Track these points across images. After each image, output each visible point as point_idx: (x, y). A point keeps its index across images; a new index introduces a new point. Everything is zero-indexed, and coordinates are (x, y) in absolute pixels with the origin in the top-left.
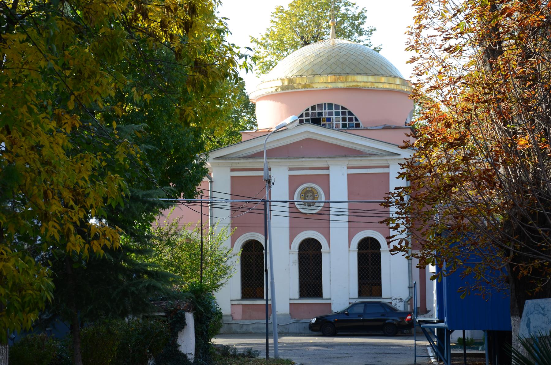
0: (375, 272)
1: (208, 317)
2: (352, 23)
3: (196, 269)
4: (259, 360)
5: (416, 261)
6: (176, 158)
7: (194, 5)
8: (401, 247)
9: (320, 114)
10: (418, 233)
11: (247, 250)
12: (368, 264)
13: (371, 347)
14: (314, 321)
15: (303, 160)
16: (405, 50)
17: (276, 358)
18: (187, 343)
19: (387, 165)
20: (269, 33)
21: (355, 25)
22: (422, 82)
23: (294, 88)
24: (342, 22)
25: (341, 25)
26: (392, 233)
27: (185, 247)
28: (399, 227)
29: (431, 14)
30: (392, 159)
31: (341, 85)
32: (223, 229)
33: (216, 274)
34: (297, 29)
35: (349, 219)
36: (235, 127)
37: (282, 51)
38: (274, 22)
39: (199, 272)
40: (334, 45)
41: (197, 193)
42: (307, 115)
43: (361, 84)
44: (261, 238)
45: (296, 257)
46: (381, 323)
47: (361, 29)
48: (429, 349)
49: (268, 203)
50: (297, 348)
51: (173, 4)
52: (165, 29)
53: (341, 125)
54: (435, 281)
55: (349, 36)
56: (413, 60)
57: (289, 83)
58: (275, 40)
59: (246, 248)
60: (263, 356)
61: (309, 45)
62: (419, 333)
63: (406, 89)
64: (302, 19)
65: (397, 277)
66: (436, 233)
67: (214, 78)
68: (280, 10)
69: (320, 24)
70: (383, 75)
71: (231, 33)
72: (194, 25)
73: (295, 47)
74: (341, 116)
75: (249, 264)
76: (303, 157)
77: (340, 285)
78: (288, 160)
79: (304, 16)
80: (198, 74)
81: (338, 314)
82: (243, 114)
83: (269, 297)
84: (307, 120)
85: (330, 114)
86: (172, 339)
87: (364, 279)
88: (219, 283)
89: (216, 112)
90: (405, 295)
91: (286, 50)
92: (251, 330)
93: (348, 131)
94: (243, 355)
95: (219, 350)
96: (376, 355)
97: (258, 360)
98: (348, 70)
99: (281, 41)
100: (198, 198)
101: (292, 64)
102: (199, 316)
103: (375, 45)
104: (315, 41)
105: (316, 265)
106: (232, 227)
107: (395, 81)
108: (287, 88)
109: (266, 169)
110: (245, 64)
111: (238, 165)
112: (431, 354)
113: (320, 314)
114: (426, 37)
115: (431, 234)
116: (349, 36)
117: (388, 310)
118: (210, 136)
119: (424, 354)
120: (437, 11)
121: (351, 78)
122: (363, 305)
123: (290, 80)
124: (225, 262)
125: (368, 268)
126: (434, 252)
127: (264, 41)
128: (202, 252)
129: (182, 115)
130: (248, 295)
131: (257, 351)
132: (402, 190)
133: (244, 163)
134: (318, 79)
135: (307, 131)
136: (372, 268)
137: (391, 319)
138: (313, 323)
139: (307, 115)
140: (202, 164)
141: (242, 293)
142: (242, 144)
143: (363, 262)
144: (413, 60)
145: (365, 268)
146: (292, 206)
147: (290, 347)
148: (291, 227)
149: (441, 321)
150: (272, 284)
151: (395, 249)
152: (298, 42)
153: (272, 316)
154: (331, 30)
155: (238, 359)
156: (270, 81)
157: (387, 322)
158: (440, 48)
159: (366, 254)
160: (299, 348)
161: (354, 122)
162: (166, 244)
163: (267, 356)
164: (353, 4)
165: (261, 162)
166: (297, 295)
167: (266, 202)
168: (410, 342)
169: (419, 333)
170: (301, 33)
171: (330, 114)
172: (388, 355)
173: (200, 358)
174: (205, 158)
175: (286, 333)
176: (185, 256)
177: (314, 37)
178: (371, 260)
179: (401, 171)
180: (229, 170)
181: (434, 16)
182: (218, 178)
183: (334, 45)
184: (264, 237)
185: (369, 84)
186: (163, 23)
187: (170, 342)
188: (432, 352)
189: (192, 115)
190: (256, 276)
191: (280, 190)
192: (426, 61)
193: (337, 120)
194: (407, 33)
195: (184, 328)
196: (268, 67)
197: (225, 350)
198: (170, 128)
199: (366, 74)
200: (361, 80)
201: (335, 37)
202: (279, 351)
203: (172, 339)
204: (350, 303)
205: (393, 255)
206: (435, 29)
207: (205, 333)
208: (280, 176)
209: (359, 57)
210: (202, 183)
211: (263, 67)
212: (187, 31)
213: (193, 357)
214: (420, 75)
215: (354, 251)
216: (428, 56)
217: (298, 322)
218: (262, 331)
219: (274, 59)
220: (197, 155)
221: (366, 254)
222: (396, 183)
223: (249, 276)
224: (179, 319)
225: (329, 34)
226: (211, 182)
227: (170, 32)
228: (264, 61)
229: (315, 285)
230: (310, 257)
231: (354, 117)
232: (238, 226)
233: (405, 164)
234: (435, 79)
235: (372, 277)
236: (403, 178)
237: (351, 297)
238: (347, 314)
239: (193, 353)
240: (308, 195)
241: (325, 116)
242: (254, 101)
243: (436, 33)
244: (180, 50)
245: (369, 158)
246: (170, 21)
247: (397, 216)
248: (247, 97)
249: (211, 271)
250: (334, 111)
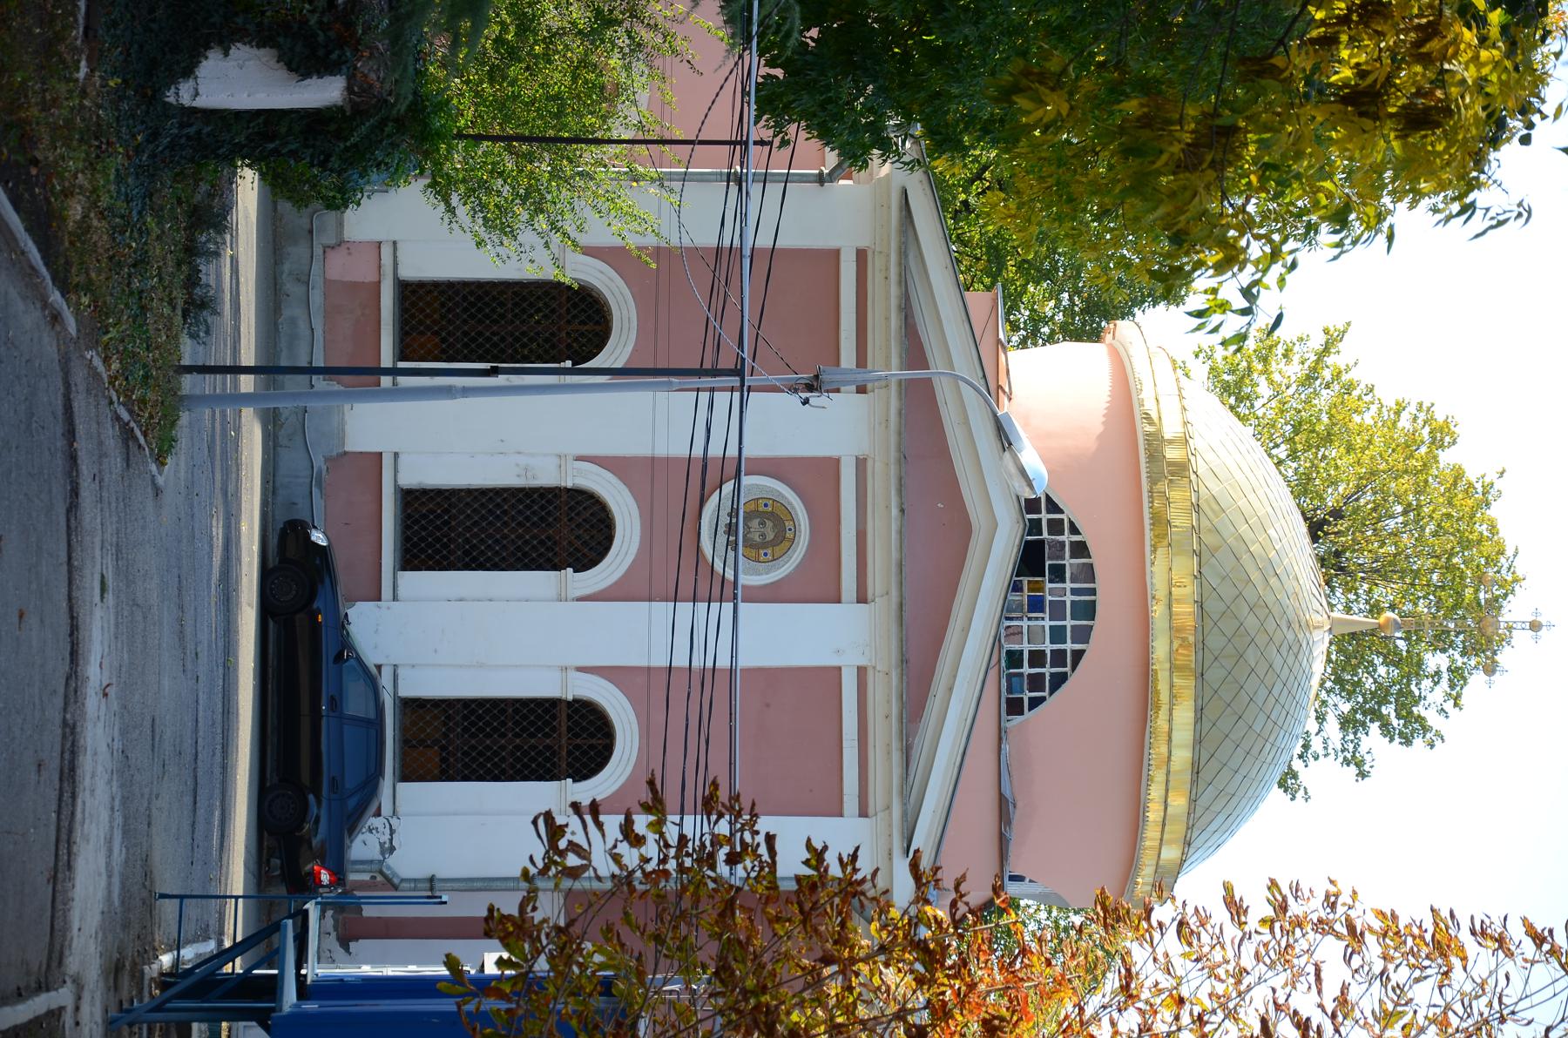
0: (489, 759)
1: (327, 160)
2: (1388, 693)
3: (507, 119)
4: (174, 338)
5: (509, 905)
6: (906, 54)
7: (1438, 125)
8: (562, 854)
9: (1058, 574)
10: (613, 913)
11: (575, 306)
12: (517, 735)
13: (219, 738)
14: (318, 537)
15: (895, 512)
16: (1273, 881)
17: (182, 398)
18: (237, 81)
19: (871, 811)
20: (1355, 393)
21: (1380, 704)
22: (1157, 936)
23: (1153, 481)
24: (1393, 659)
25: (1378, 653)
26: (613, 823)
27: (586, 82)
28: (632, 845)
29: (1401, 975)
30: (890, 825)
31: (1160, 649)
32: (651, 218)
33: (489, 191)
34: (1369, 496)
35: (680, 669)
36: (1019, 267)
37: (1290, 440)
38: (1398, 413)
39: (497, 130)
40: (1309, 627)
41: (779, 128)
42: (1056, 527)
43: (1162, 722)
44: (614, 354)
45: (546, 477)
46: (305, 778)
47: (1363, 724)
48: (210, 947)
49: (735, 381)
50: (218, 476)
51: (1446, 47)
52: (1355, 17)
53: (1017, 647)
54: (443, 971)
55: (1341, 681)
56: (1236, 909)
57: (1170, 464)
58: (1331, 417)
59: (583, 299)
60: (189, 352)
61: (1307, 540)
62: (269, 914)
63: (1144, 879)
64: (1405, 513)
65: (460, 835)
66: (616, 976)
67: (1172, 195)
68: (1442, 436)
69: (1385, 578)
70: (1193, 801)
71: (1335, 258)
72: (1368, 123)
73: (1302, 488)
74: (1048, 647)
75: (524, 311)
76: (902, 511)
77: (444, 635)
78: (893, 454)
79: (1417, 522)
80: (1188, 138)
81: (342, 624)
82: (1066, 295)
83: (404, 381)
84: (1035, 527)
85: (1058, 610)
86: (251, 28)
87: (465, 718)
88: (455, 200)
89: (1070, 200)
90: (408, 864)
91: (1293, 455)
92: (287, 313)
93: (993, 673)
94: (193, 281)
95: (211, 196)
96: (189, 758)
97: (176, 337)
98: (1214, 675)
99: (1328, 439)
100: (761, 131)
101: (1240, 475)
102: (333, 127)
103: (1308, 775)
104: (1322, 561)
105: (518, 548)
106: (658, 252)
107: (1171, 842)
108: (1155, 455)
109: (866, 376)
110: (1224, 307)
111: (879, 277)
112: (188, 953)
113: (340, 560)
114: (1317, 957)
115: (611, 958)
116: (1339, 681)
117: (352, 803)
118: (987, 174)
119: (189, 928)
120: (1410, 995)
121: (1186, 684)
122: (372, 715)
123: (1181, 469)
124: (530, 222)
125: (503, 735)
126: (542, 965)
127: (1327, 374)
128: (569, 141)
129: (1042, 78)
130: (413, 304)
131: (207, 332)
132: (766, 857)
133: (888, 298)
134: (1184, 568)
135: (995, 525)
136: (503, 748)
137: (320, 812)
138: (308, 537)
139: (1056, 527)
140: (886, 147)
141: (421, 285)
142: (954, 291)
143: (525, 717)
144: (1236, 909)
145: (503, 724)
146: (730, 469)
147: (224, 452)
148: (653, 464)
149: (304, 990)
150: (448, 392)
151: (555, 832)
152: (1322, 499)
153: (337, 387)
154: (1360, 618)
155: (179, 265)
156: (1181, 397)
157: (311, 797)
158: (1278, 1007)
159: (554, 729)
160: (218, 484)
162: (598, 12)
163: (190, 369)
164: (1457, 698)
165: (888, 358)
166: (409, 479)
167: (738, 372)
168: (237, 878)
169: (269, 914)
170: (1356, 510)
171: (1058, 610)
172: (188, 799)
173: (182, 126)
174: (906, 159)
175: (276, 437)
176: (557, 77)
177: (1338, 554)
178: (533, 747)
179: (831, 858)
180: (863, 244)
181: (1393, 983)
182: (838, 205)
183: (1309, 627)
184: (619, 365)
185: (1164, 749)
186: (1378, 13)
187: (239, 20)
188: (198, 955)
189: (1039, 113)
190: (480, 334)
191: (780, 424)
192: (1230, 954)
193: (1035, 634)
194: (1333, 889)
195: (290, 69)
196: (1234, 391)
197: (211, 217)
198: (1020, 29)
199: (1198, 741)
200: (1178, 721)
201: (1338, 631)
202: (207, 411)
203: (251, 28)
204: (379, 667)
205: (535, 822)
206: (1345, 988)
207: (271, 146)
208: (836, 426)
209: (1262, 718)
210: (816, 144)
211: (1232, 372)
212: (1345, 100)
213: (186, 100)
214: (1179, 932)
215: (565, 685)
216: (1247, 961)
217: (315, 480)
218: (284, 354)
219: (1260, 413)
220: (918, 130)
221: (554, 729)
222: (792, 840)
223: (480, 310)
224: (321, 53)
225: (1348, 609)
226: (821, 179)
227: (1344, 38)
228: (1255, 376)
229: (445, 546)
230: (544, 529)
231: (1045, 694)
232: (657, 269)
233: (855, 870)
234: (1166, 982)
235: (473, 748)
236: (807, 863)
237: (400, 671)
238: (339, 658)
239: (200, 103)
240: (769, 524)
241: (1051, 592)
242: (1109, 337)
243: (1331, 990)
244: (1274, 72)
245: (895, 745)
246: (1381, 35)
247: (673, 839)
248: (1126, 314)
249: (501, 174)
250: (1069, 623)
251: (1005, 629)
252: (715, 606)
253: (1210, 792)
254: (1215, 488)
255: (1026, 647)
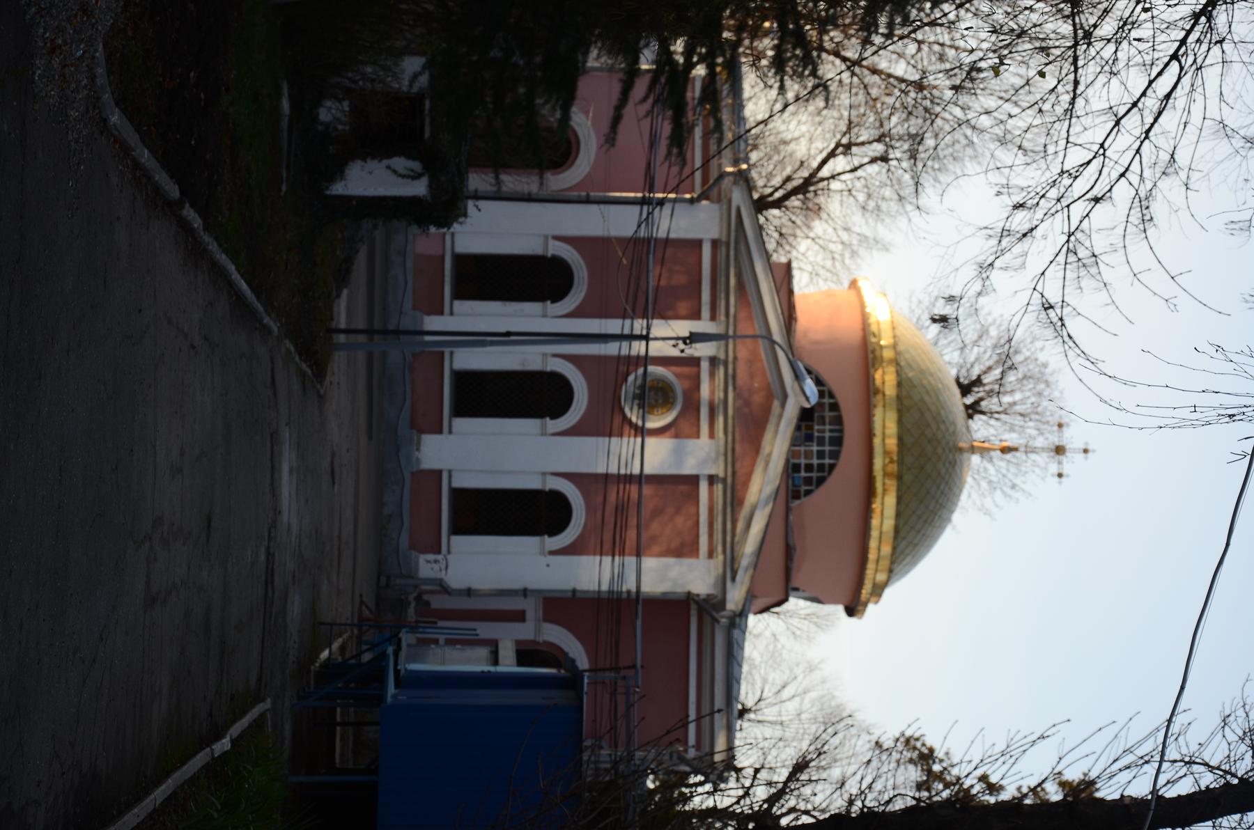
31: (878, 463)
53: (796, 461)
70: (894, 548)
74: (815, 461)
90: (456, 579)
98: (908, 478)
121: (892, 485)
161: (804, 488)
171: (821, 442)
199: (898, 515)
200: (886, 508)
215: (544, 482)
237: (453, 474)
241: (818, 431)
251: (791, 454)
252: (632, 439)
253: (904, 543)
254: (911, 374)
255: (803, 461)
